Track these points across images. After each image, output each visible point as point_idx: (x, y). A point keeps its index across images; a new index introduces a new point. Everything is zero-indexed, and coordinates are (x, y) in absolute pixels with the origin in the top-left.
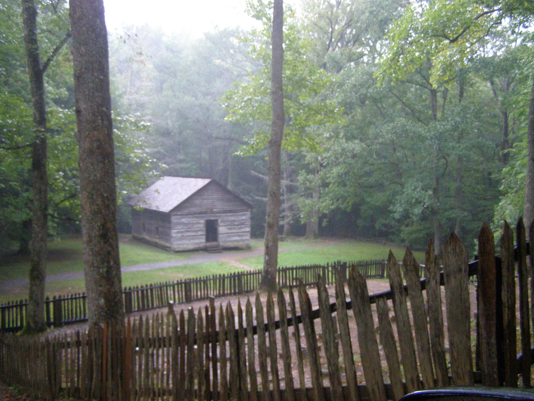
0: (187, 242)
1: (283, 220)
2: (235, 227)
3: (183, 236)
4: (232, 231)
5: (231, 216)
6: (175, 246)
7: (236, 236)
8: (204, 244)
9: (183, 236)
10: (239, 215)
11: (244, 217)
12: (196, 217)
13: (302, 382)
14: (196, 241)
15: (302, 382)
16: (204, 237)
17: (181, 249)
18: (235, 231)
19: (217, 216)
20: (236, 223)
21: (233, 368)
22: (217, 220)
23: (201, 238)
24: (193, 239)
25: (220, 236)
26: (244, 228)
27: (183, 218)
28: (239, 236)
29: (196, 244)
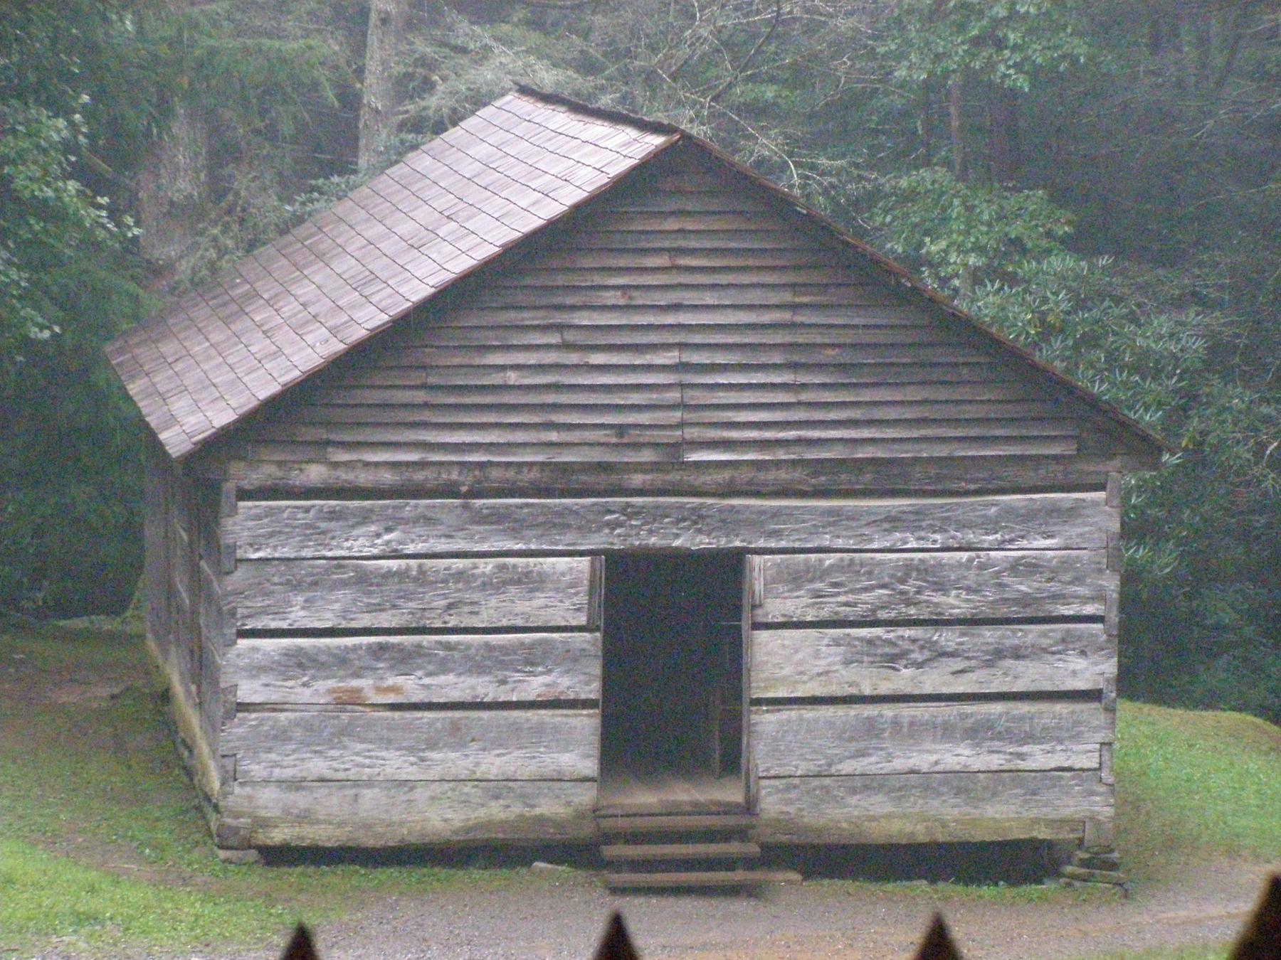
0: (396, 764)
1: (914, 717)
2: (948, 638)
3: (347, 701)
4: (903, 679)
5: (894, 521)
6: (269, 800)
7: (946, 732)
8: (586, 796)
9: (347, 701)
10: (991, 525)
11: (1041, 546)
12: (497, 518)
13: (564, 587)
14: (494, 764)
15: (564, 587)
16: (586, 724)
17: (324, 835)
18: (934, 680)
19: (729, 522)
20: (955, 603)
21: (633, 432)
22: (734, 562)
23: (563, 740)
24: (457, 738)
25: (766, 722)
26: (1038, 652)
27: (365, 518)
28: (977, 733)
29: (500, 787)
